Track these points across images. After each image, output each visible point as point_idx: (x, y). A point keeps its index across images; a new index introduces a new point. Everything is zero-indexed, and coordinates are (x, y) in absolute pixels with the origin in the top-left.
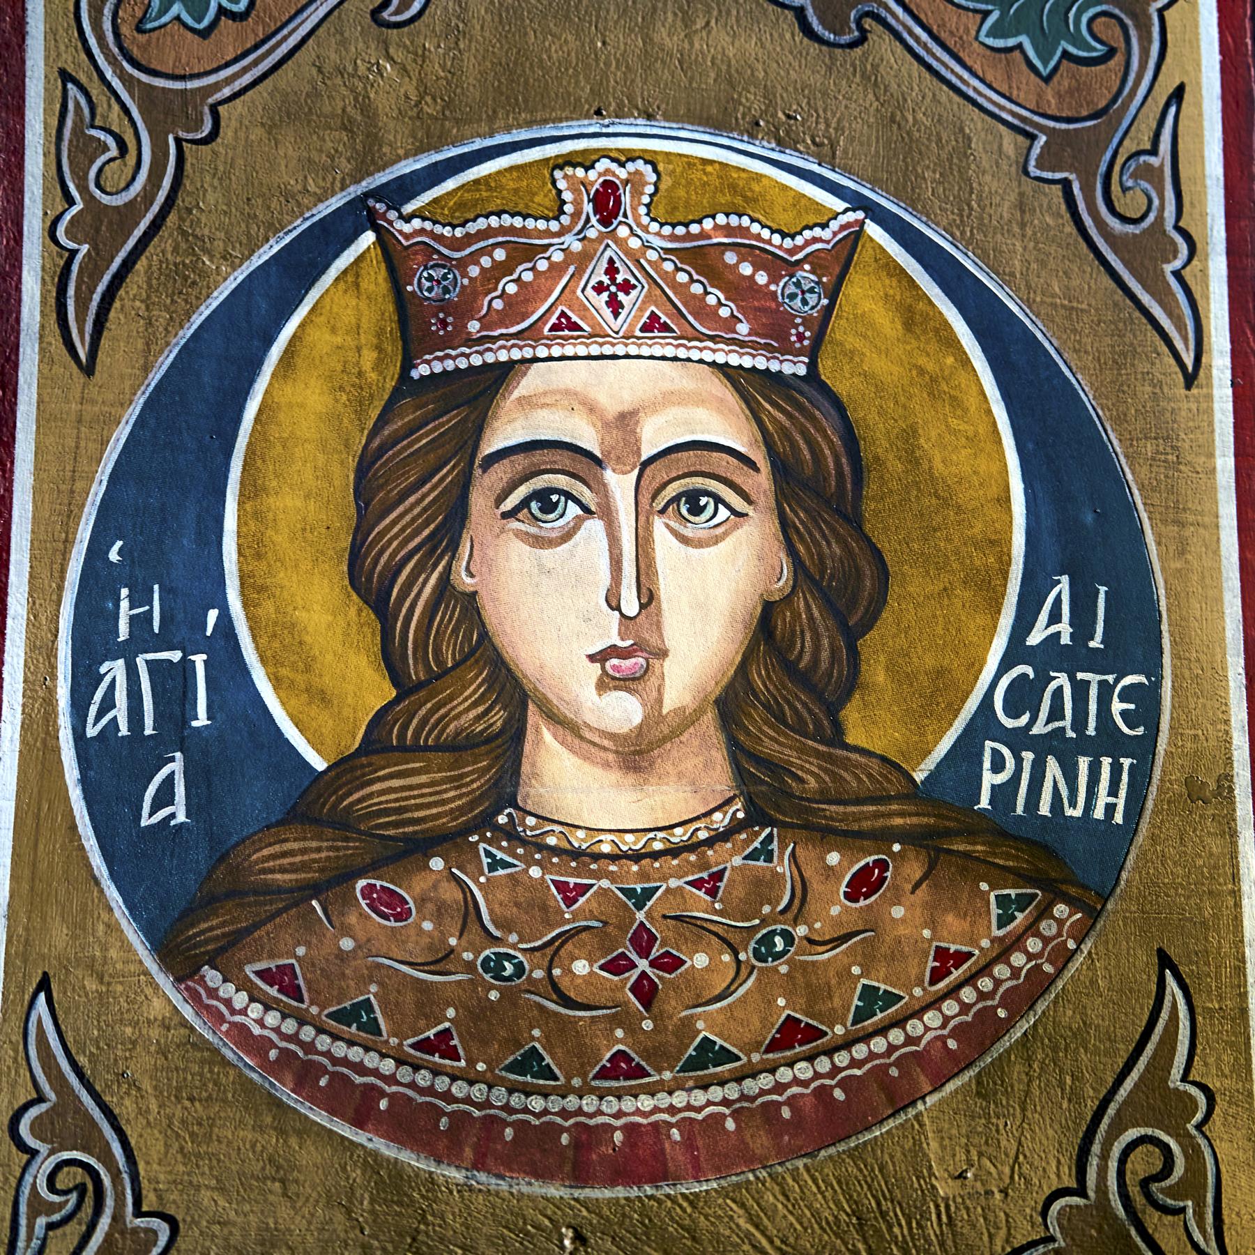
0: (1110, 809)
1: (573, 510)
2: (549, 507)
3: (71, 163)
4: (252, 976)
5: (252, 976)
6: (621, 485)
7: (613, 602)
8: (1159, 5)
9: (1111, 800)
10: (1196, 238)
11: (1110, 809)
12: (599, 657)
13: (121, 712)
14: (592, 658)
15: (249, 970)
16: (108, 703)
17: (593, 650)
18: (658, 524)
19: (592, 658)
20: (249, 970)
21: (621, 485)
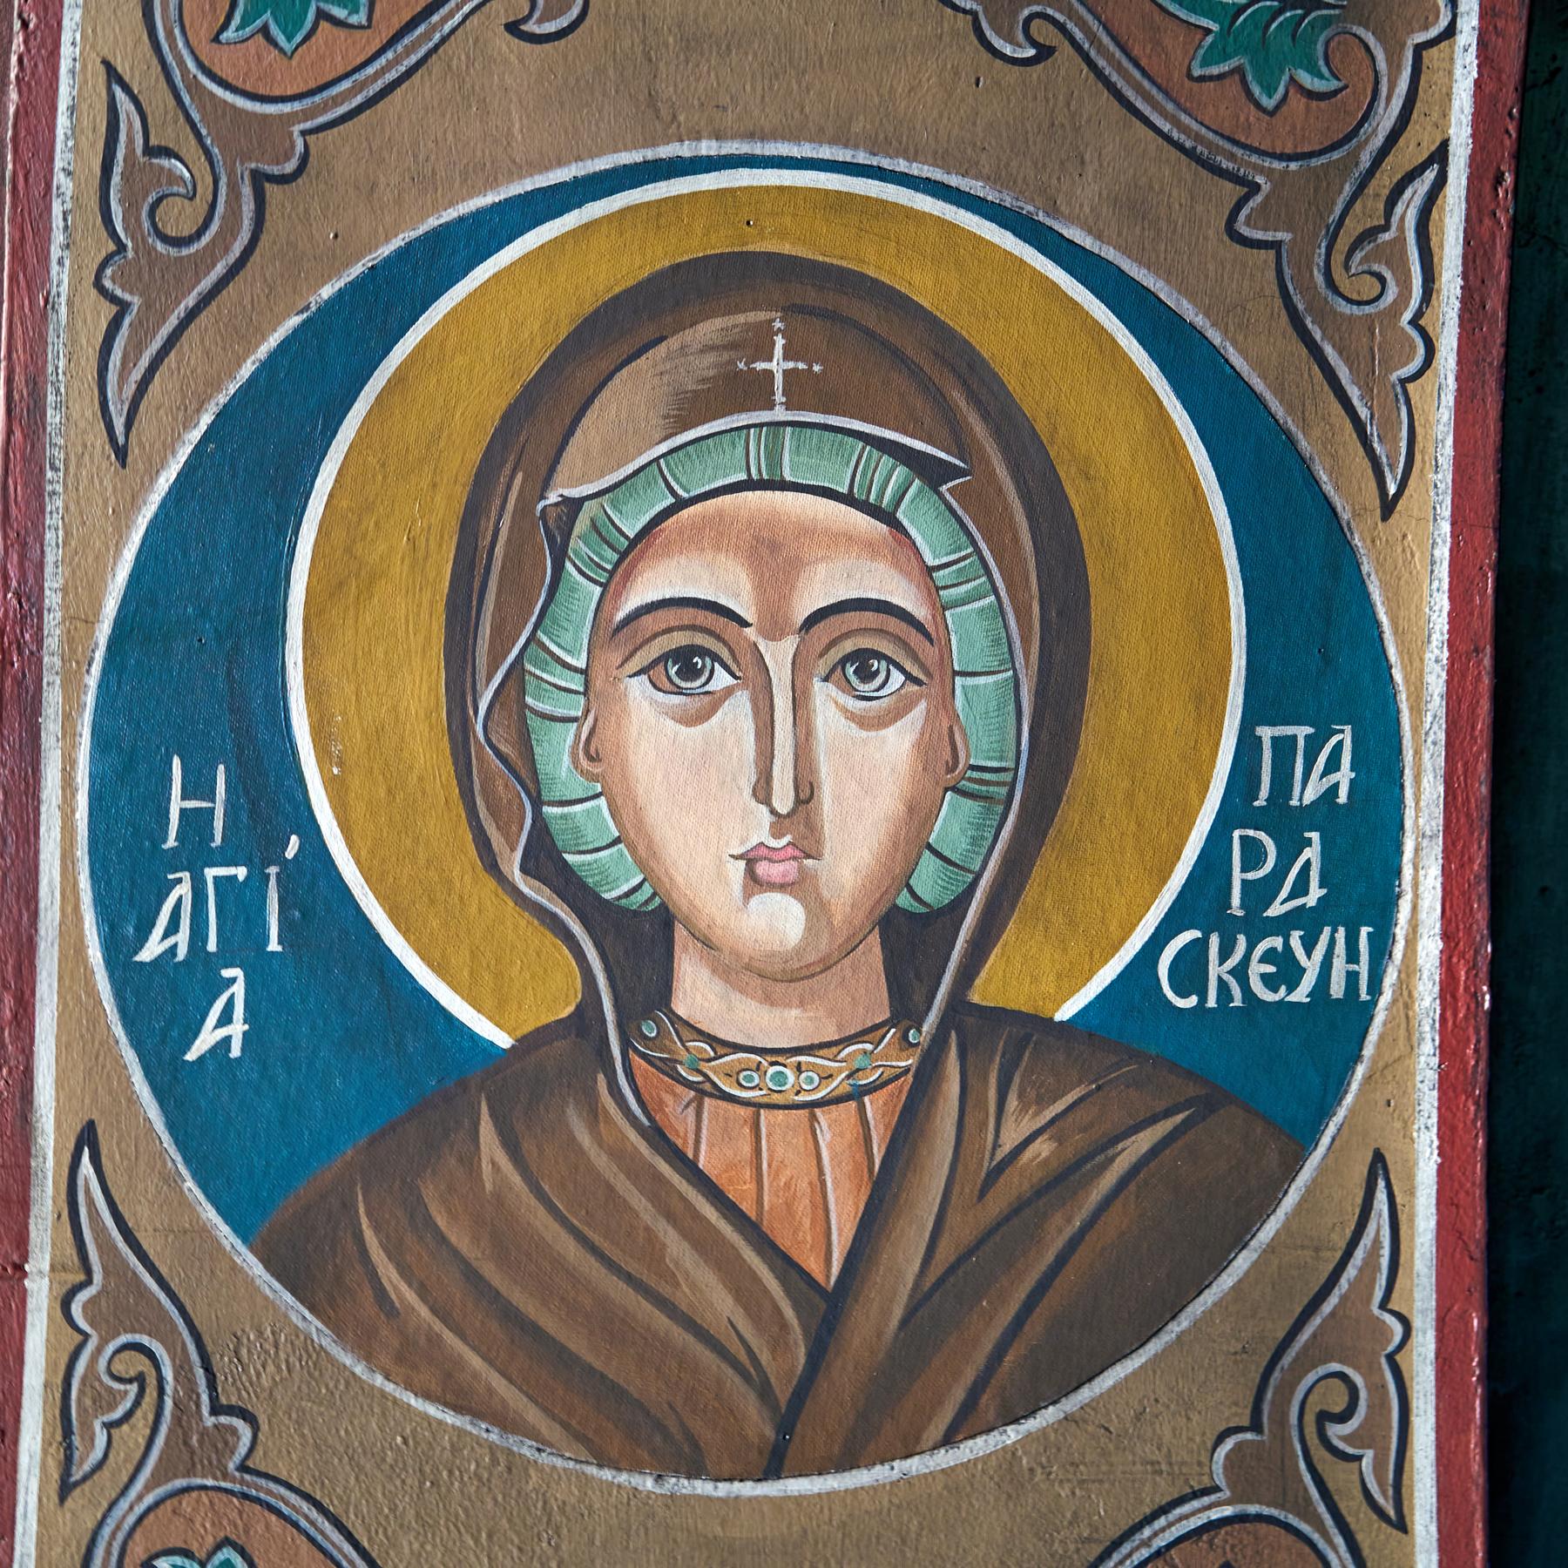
6: (779, 656)
7: (762, 792)
13: (182, 938)
14: (747, 896)
19: (747, 896)
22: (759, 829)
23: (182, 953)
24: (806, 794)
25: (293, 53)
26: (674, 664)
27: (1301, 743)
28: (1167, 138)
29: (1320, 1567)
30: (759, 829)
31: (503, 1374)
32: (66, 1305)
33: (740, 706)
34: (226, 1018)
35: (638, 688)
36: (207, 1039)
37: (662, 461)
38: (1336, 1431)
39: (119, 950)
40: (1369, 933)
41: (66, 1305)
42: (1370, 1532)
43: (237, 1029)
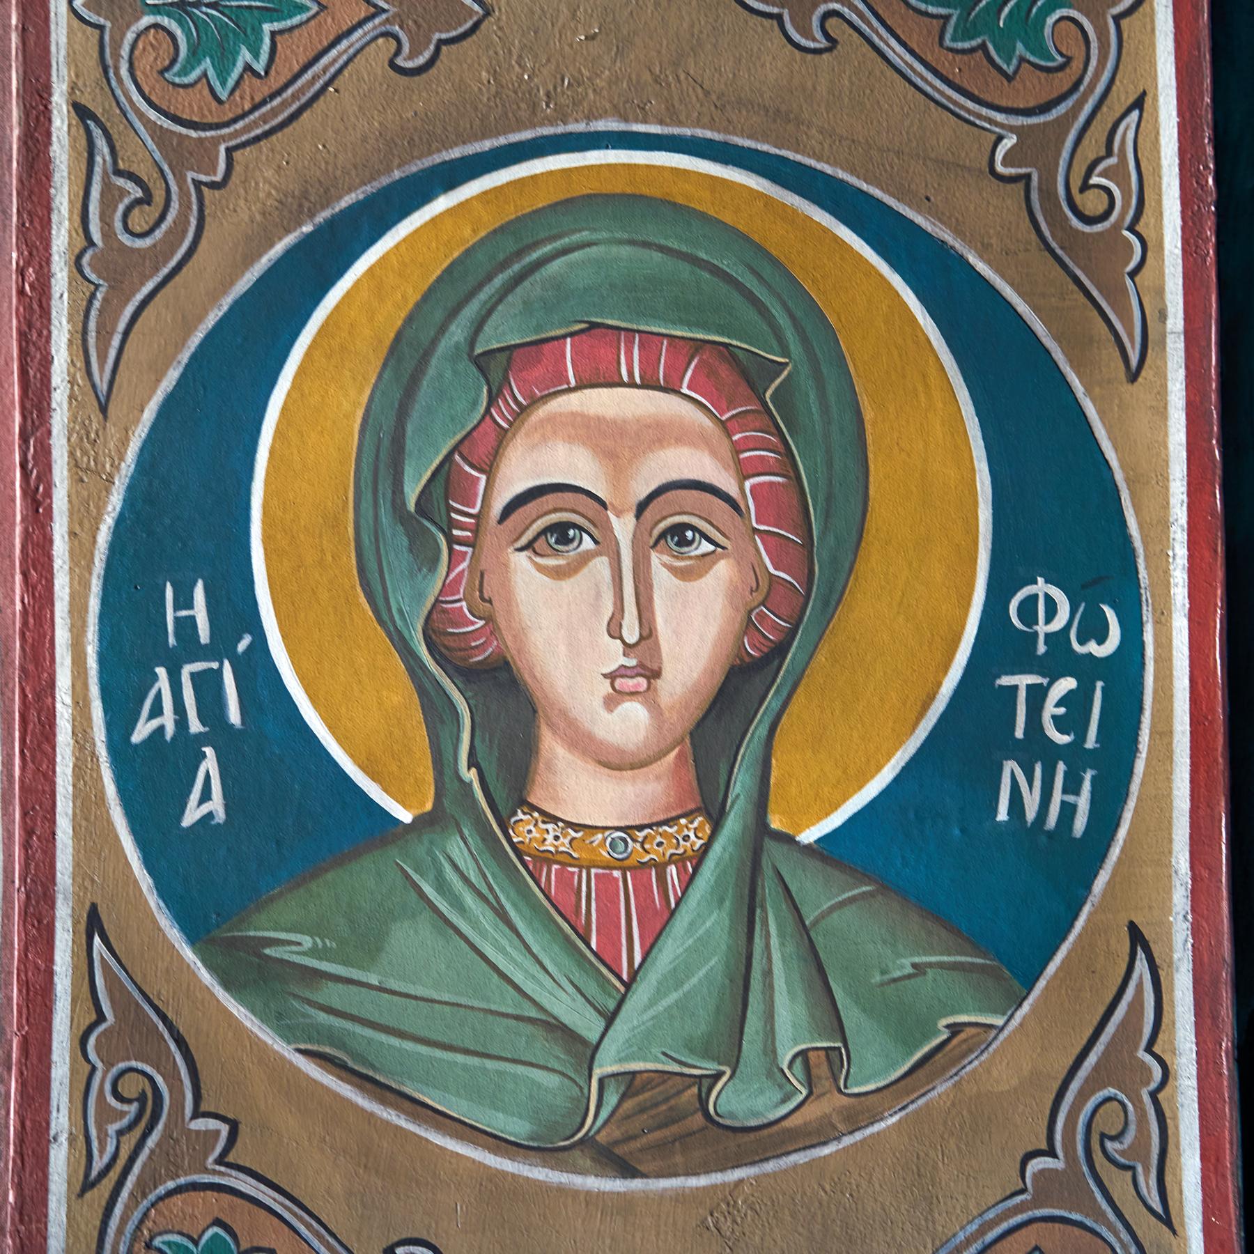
0: (1068, 811)
1: (588, 544)
2: (564, 540)
3: (173, 253)
4: (189, 180)
5: (189, 180)
6: (623, 528)
7: (614, 630)
8: (1117, 10)
9: (1070, 798)
10: (1145, 236)
11: (1068, 811)
12: (611, 677)
13: (168, 719)
14: (605, 676)
15: (190, 175)
16: (157, 711)
17: (607, 670)
18: (656, 559)
19: (605, 676)
20: (190, 175)
21: (623, 528)
22: (615, 657)
23: (170, 731)
24: (648, 634)
25: (267, 73)
26: (552, 536)
27: (1022, 695)
28: (878, 1090)
29: (1110, 1253)
30: (615, 657)
31: (144, 126)
32: (83, 1041)
33: (601, 565)
34: (206, 796)
35: (521, 561)
36: (191, 816)
37: (622, 989)
38: (1109, 1145)
39: (120, 722)
40: (1093, 776)
41: (83, 1041)
42: (1147, 1228)
43: (216, 804)
